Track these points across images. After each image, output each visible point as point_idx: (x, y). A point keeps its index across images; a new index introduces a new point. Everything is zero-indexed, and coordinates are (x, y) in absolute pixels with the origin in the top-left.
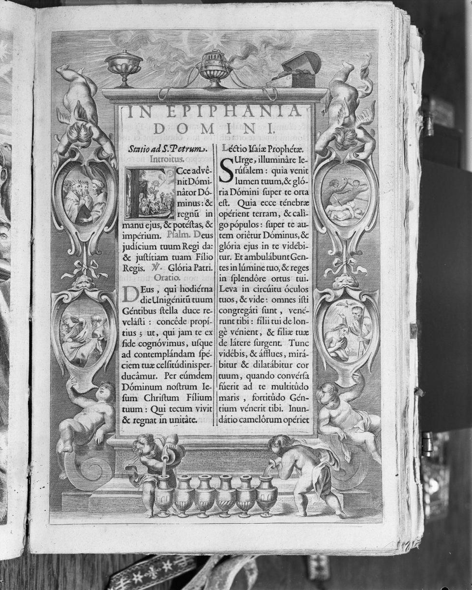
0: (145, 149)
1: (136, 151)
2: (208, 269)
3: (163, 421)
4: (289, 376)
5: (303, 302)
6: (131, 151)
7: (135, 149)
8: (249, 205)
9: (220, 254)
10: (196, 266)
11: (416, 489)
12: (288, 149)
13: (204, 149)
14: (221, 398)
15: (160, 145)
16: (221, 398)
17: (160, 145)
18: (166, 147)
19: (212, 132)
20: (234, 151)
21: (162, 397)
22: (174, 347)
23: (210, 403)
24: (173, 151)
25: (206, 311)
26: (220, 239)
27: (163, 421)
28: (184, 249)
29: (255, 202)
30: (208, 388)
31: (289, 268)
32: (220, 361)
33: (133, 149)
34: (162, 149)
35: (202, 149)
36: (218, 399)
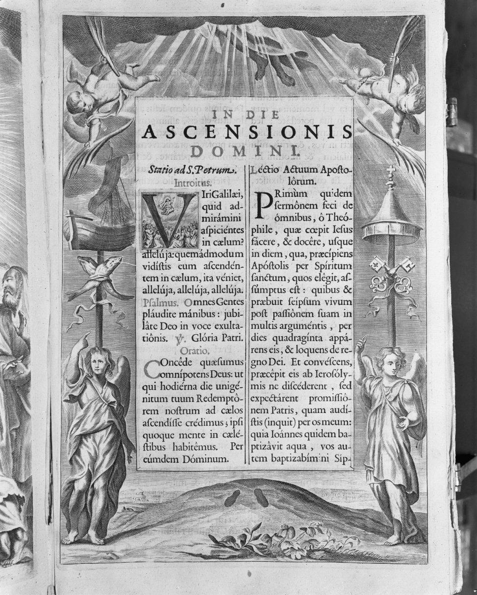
0: (167, 169)
1: (157, 172)
4: (317, 362)
6: (151, 171)
7: (156, 169)
9: (252, 370)
10: (225, 336)
11: (454, 535)
12: (337, 216)
13: (233, 170)
14: (254, 326)
15: (185, 166)
16: (253, 386)
17: (185, 166)
18: (191, 167)
19: (244, 155)
22: (215, 258)
23: (241, 368)
24: (198, 173)
25: (239, 375)
26: (251, 294)
28: (198, 401)
33: (153, 169)
34: (187, 170)
35: (231, 170)
36: (250, 412)
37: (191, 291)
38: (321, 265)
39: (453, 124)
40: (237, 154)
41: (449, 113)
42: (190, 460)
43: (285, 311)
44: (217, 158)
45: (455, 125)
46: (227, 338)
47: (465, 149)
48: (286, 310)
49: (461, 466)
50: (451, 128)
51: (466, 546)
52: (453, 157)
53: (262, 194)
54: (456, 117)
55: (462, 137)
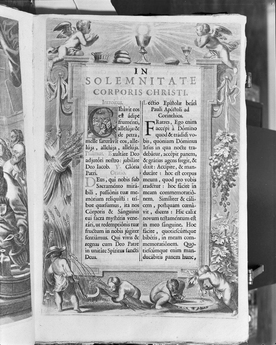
2: (95, 174)
3: (169, 116)
5: (122, 200)
8: (118, 239)
10: (129, 243)
20: (152, 104)
21: (121, 198)
27: (169, 116)
29: (129, 205)
30: (136, 142)
31: (173, 135)
32: (143, 235)
37: (108, 148)
38: (111, 250)
39: (249, 87)
40: (128, 82)
41: (247, 81)
42: (180, 142)
43: (106, 191)
44: (99, 77)
45: (250, 87)
46: (130, 244)
47: (256, 100)
48: (107, 191)
49: (253, 271)
50: (248, 89)
51: (256, 317)
52: (248, 103)
53: (149, 122)
54: (251, 83)
55: (254, 94)
